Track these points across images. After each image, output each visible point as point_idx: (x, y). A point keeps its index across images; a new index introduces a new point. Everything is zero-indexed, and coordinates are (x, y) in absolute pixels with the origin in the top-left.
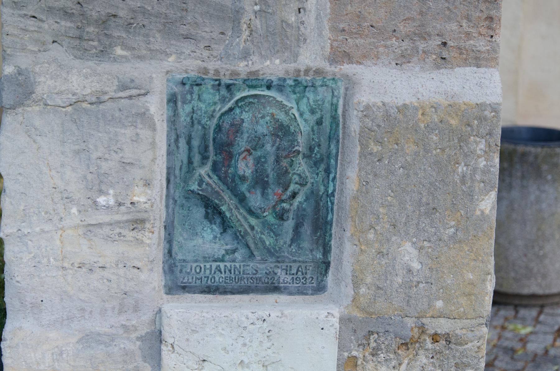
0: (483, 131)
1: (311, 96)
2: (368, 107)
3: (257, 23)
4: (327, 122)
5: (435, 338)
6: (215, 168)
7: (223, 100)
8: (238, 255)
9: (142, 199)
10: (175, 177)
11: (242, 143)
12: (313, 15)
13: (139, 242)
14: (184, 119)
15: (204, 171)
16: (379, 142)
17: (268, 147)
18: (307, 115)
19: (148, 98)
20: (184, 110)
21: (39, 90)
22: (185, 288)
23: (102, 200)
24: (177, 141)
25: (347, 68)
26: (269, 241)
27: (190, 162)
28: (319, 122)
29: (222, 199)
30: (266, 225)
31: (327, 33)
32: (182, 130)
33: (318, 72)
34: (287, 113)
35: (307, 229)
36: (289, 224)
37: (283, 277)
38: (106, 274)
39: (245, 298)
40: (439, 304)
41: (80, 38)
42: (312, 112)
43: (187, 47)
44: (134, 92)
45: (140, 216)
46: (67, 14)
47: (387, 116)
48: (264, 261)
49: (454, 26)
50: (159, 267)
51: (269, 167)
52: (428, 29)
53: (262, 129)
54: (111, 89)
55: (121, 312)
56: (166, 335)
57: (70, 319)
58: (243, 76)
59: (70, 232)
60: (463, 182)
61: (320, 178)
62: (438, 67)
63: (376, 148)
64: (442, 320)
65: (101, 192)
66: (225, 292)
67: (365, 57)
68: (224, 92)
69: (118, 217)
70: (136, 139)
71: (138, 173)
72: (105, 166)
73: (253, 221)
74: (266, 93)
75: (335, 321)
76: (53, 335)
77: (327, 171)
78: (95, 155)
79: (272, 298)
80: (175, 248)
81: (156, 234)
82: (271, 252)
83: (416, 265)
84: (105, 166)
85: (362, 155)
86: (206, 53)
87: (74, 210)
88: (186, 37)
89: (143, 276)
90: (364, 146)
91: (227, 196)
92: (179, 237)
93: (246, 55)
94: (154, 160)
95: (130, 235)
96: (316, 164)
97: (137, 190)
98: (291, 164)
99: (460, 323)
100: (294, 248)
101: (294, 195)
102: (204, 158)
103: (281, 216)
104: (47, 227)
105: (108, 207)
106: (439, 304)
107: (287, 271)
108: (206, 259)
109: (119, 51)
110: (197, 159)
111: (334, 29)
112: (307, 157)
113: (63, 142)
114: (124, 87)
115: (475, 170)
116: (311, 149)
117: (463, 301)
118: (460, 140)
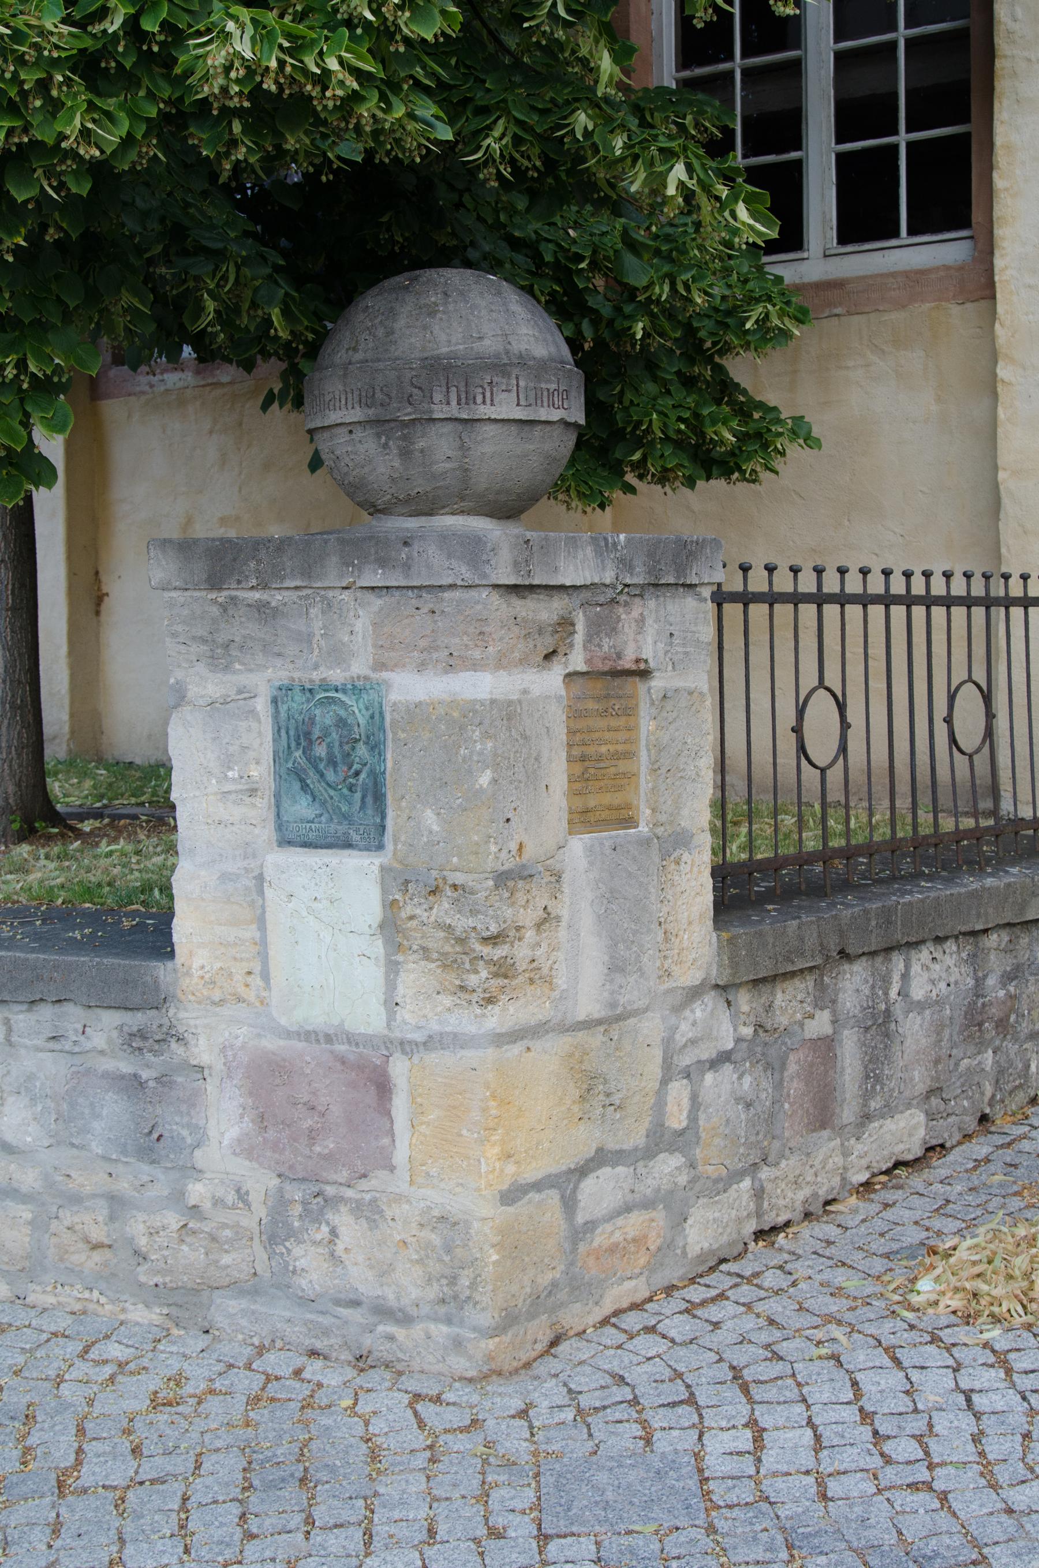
0: (477, 722)
1: (365, 696)
2: (395, 704)
3: (323, 643)
4: (377, 716)
5: (455, 887)
6: (304, 753)
7: (308, 701)
8: (323, 819)
9: (256, 774)
10: (814, 815)
11: (316, 733)
12: (360, 635)
13: (254, 805)
14: (283, 715)
15: (298, 754)
16: (403, 731)
17: (334, 735)
18: (364, 711)
19: (256, 699)
20: (283, 709)
21: (190, 695)
22: (290, 843)
23: (230, 774)
24: (279, 731)
25: (385, 675)
26: (344, 808)
27: (289, 747)
28: (372, 717)
29: (307, 775)
30: (342, 795)
31: (370, 649)
32: (283, 724)
33: (366, 678)
34: (346, 710)
35: (369, 800)
36: (358, 796)
37: (355, 837)
38: (234, 828)
39: (330, 851)
40: (455, 860)
41: (212, 657)
42: (367, 709)
43: (279, 662)
44: (247, 695)
45: (255, 786)
46: (204, 641)
47: (408, 710)
48: (340, 823)
49: (457, 640)
50: (271, 825)
51: (336, 750)
52: (439, 643)
53: (328, 722)
54: (232, 693)
55: (246, 857)
56: (265, 875)
57: (214, 861)
58: (318, 683)
59: (211, 797)
60: (464, 760)
61: (375, 760)
62: (447, 673)
63: (403, 736)
64: (458, 874)
65: (230, 768)
66: (316, 847)
67: (396, 666)
68: (308, 695)
69: (240, 787)
70: (249, 730)
71: (251, 754)
72: (231, 749)
73: (332, 793)
74: (336, 695)
75: (376, 869)
76: (203, 873)
77: (380, 754)
78: (225, 741)
79: (347, 852)
80: (282, 812)
81: (266, 800)
82: (345, 816)
83: (435, 828)
84: (231, 749)
85: (393, 740)
86: (291, 666)
87: (214, 781)
88: (279, 655)
89: (257, 831)
90: (395, 734)
91: (311, 773)
92: (286, 803)
93: (316, 667)
94: (261, 744)
95: (248, 800)
96: (373, 749)
97: (253, 766)
98: (353, 748)
99: (471, 877)
100: (361, 814)
101: (357, 774)
102: (298, 744)
103: (351, 788)
104: (197, 793)
105: (234, 779)
106: (455, 860)
107: (357, 831)
108: (302, 821)
109: (237, 666)
110: (293, 745)
111: (375, 646)
112: (366, 743)
113: (204, 732)
114: (240, 692)
115: (472, 753)
116: (368, 737)
117: (472, 858)
118: (461, 728)
